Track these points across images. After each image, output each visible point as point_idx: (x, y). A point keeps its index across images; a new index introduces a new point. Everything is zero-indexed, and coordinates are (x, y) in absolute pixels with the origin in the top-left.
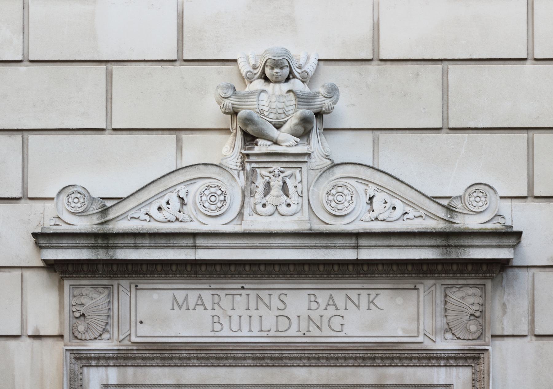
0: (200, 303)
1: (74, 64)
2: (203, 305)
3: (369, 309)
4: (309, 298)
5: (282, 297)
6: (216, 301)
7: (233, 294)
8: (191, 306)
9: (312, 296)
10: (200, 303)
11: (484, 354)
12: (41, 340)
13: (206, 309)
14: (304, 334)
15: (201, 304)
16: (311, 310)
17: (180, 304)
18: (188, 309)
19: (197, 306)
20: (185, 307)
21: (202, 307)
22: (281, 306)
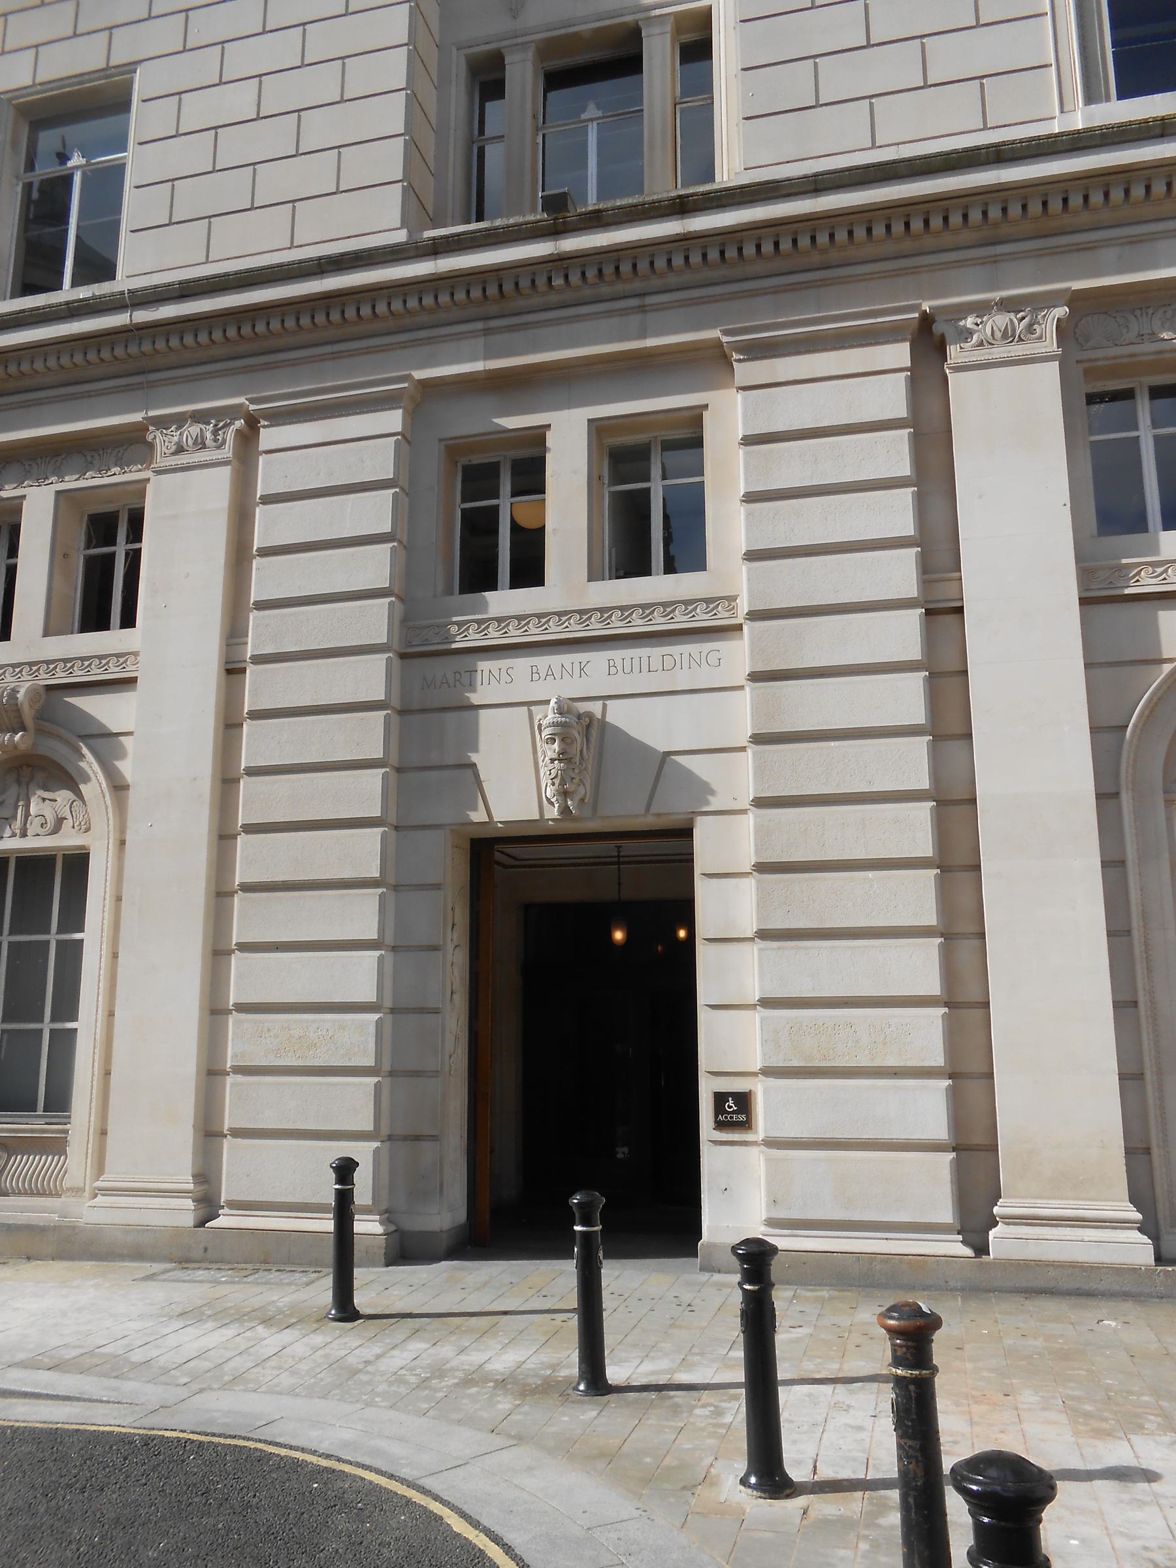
0: (550, 673)
2: (447, 683)
18: (435, 688)
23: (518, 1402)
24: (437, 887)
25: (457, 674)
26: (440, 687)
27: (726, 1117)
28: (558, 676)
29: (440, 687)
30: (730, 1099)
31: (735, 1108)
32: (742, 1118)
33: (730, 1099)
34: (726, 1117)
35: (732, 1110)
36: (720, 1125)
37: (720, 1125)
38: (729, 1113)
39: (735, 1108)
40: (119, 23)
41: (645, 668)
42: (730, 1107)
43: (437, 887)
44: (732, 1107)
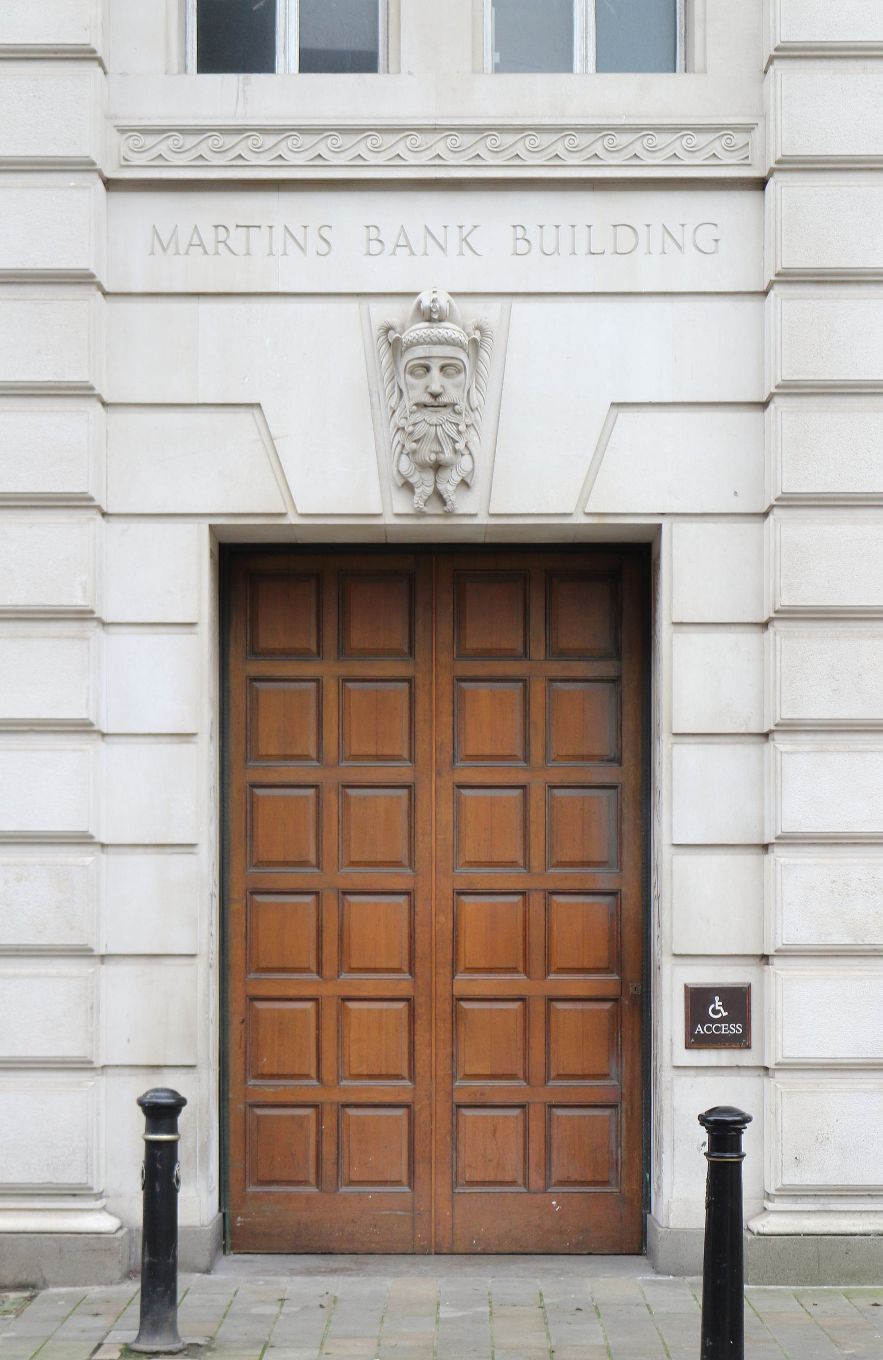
0: (402, 242)
1: (492, 168)
2: (201, 245)
3: (461, 254)
4: (515, 234)
5: (325, 232)
6: (519, 235)
7: (248, 227)
8: (183, 248)
9: (372, 229)
10: (402, 242)
11: (783, 1058)
12: (872, 1198)
13: (412, 253)
14: (435, 396)
15: (199, 243)
16: (517, 254)
17: (165, 244)
18: (177, 253)
19: (398, 249)
20: (171, 249)
21: (406, 249)
22: (324, 248)
23: (91, 970)
24: (186, 737)
25: (372, 229)
26: (187, 253)
27: (709, 1029)
28: (418, 249)
29: (187, 253)
30: (717, 998)
31: (725, 1014)
32: (736, 1029)
33: (717, 998)
34: (709, 1029)
35: (720, 1015)
36: (694, 1041)
37: (694, 1041)
38: (714, 1021)
39: (725, 1014)
40: (169, 1063)
41: (581, 248)
42: (715, 1012)
43: (186, 737)
44: (719, 1011)
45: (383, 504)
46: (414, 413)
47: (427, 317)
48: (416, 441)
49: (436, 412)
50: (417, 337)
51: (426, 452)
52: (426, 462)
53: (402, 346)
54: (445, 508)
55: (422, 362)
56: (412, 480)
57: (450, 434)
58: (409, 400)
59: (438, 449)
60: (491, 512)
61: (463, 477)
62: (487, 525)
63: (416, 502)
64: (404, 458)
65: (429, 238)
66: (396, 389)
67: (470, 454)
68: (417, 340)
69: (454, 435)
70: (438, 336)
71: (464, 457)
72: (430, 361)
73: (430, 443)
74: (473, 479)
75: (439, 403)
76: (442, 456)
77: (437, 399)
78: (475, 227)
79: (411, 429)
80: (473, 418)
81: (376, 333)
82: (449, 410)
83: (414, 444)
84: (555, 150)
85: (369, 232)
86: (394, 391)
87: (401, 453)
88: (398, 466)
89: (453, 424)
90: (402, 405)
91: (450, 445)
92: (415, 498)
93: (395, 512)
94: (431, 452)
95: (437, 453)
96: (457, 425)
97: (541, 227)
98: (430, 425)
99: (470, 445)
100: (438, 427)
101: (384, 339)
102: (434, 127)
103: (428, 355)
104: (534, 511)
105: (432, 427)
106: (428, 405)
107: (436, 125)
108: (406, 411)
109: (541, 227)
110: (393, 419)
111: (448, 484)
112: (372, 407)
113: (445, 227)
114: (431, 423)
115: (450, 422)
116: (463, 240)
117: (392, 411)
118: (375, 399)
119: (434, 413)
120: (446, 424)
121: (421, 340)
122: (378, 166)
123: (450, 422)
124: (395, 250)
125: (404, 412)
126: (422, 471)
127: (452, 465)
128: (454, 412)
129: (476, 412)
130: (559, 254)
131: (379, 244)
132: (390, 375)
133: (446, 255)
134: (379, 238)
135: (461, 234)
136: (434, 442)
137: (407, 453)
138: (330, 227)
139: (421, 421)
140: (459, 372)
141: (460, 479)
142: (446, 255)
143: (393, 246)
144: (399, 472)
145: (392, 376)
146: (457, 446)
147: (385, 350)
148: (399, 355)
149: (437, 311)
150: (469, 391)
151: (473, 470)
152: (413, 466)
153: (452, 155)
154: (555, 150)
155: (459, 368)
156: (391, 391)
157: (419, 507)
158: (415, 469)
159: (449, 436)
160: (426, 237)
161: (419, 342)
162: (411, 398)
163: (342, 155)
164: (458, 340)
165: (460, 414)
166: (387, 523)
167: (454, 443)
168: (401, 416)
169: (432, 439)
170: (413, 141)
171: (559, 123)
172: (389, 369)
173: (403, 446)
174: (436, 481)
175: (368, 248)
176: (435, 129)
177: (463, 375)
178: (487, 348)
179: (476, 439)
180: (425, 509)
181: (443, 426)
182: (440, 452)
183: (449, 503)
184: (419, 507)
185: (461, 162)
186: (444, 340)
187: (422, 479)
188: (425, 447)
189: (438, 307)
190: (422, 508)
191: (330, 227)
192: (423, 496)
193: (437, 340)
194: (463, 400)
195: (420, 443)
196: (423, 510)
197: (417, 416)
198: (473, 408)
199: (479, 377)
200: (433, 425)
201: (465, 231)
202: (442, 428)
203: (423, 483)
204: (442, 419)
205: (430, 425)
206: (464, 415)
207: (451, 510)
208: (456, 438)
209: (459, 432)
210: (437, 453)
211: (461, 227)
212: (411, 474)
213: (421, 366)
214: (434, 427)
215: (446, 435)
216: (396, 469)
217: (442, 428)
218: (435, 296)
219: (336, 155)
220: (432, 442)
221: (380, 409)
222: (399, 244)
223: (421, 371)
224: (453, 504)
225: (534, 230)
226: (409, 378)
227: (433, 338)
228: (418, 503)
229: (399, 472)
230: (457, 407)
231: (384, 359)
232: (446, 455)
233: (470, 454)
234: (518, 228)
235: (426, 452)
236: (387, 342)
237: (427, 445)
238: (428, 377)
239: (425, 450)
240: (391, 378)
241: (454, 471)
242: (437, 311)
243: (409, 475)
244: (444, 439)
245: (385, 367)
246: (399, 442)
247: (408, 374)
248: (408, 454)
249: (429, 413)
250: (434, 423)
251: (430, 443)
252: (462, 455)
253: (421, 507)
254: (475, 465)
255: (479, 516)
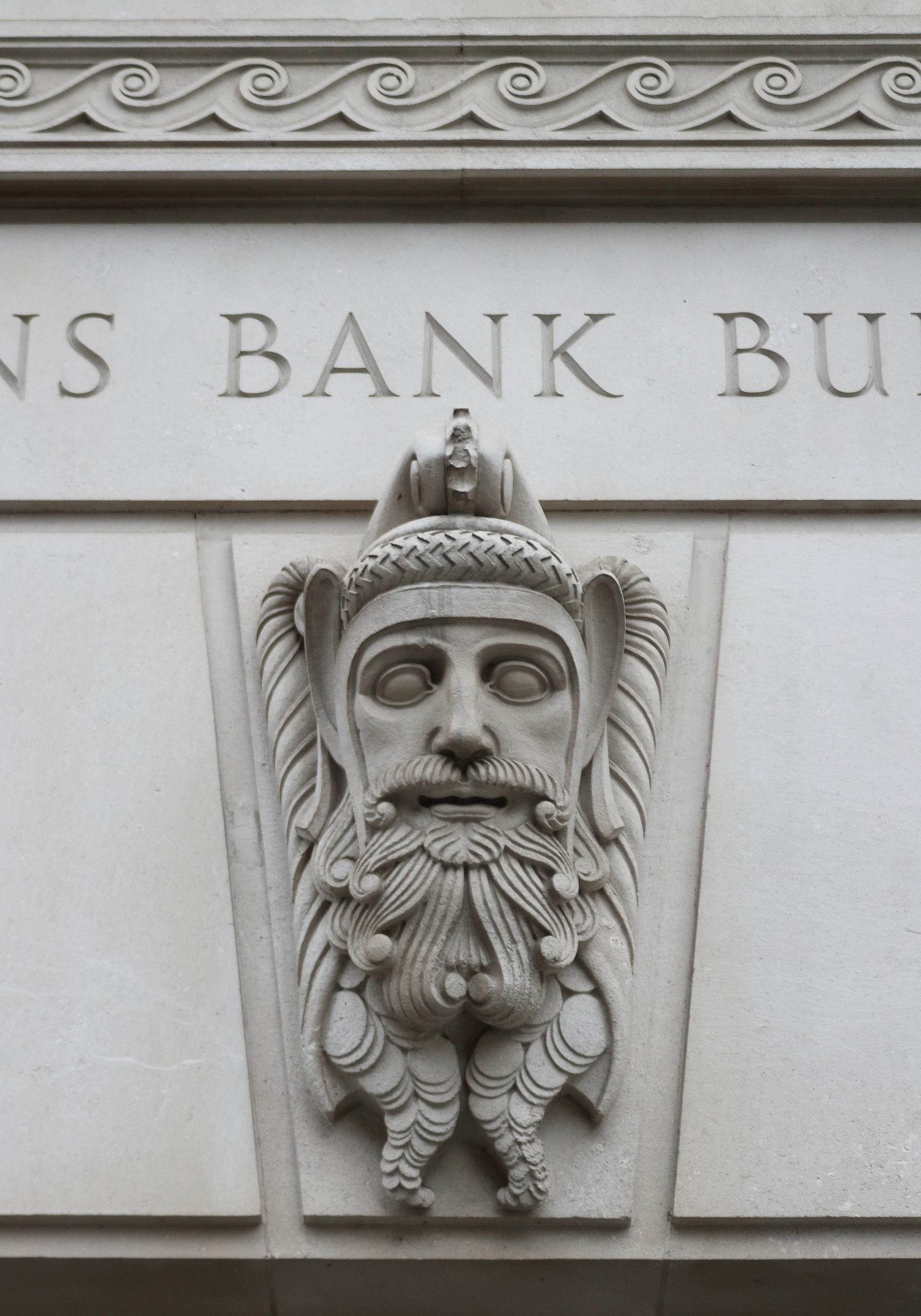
0: (350, 357)
4: (732, 337)
5: (88, 333)
10: (350, 357)
45: (262, 1184)
46: (385, 829)
47: (431, 497)
48: (392, 930)
49: (466, 821)
50: (394, 554)
51: (430, 965)
52: (430, 1004)
53: (342, 599)
54: (503, 1195)
55: (413, 639)
56: (376, 1085)
57: (521, 902)
58: (366, 787)
59: (476, 957)
60: (683, 1210)
61: (572, 1077)
62: (666, 1263)
63: (389, 1168)
64: (346, 1003)
65: (440, 348)
66: (321, 770)
67: (598, 992)
68: (394, 563)
69: (537, 907)
70: (471, 548)
71: (574, 1000)
72: (443, 638)
73: (443, 937)
74: (611, 1088)
75: (478, 784)
76: (491, 982)
77: (472, 772)
78: (596, 318)
79: (372, 883)
80: (605, 866)
81: (251, 611)
82: (517, 819)
83: (384, 939)
84: (855, 103)
85: (239, 335)
86: (312, 789)
87: (336, 987)
88: (321, 1036)
89: (530, 871)
90: (341, 817)
91: (521, 947)
92: (389, 1153)
93: (308, 1212)
94: (450, 969)
95: (470, 973)
96: (547, 872)
97: (818, 318)
98: (447, 867)
99: (596, 958)
100: (473, 876)
101: (282, 626)
102: (457, 43)
103: (435, 613)
104: (847, 1209)
105: (450, 875)
106: (435, 794)
107: (462, 37)
108: (355, 837)
109: (818, 318)
110: (305, 875)
111: (515, 1096)
112: (232, 856)
113: (496, 318)
114: (446, 856)
115: (522, 861)
116: (555, 354)
117: (303, 849)
118: (244, 830)
119: (459, 825)
120: (504, 863)
121: (412, 564)
122: (273, 144)
123: (522, 861)
124: (323, 381)
125: (350, 834)
126: (414, 1050)
127: (529, 1026)
128: (536, 824)
129: (614, 849)
130: (885, 394)
131: (271, 364)
132: (301, 735)
133: (499, 396)
134: (272, 349)
135: (551, 340)
136: (459, 936)
137: (356, 982)
138: (109, 318)
139: (410, 856)
140: (550, 685)
141: (558, 1081)
142: (499, 396)
143: (319, 371)
144: (325, 1058)
145: (307, 739)
146: (548, 946)
147: (282, 659)
148: (332, 632)
149: (470, 467)
150: (586, 773)
151: (608, 1053)
152: (380, 1029)
153: (513, 116)
154: (855, 103)
155: (553, 667)
156: (302, 785)
157: (400, 1186)
158: (387, 1038)
159: (516, 908)
160: (429, 348)
161: (401, 569)
162: (371, 778)
163: (157, 118)
164: (546, 566)
165: (557, 834)
166: (278, 1254)
167: (535, 938)
168: (334, 854)
169: (449, 921)
170: (390, 82)
171: (860, 31)
172: (297, 718)
173: (344, 960)
174: (466, 1091)
175: (235, 376)
176: (461, 50)
177: (563, 700)
178: (649, 653)
179: (615, 940)
180: (426, 1196)
181: (494, 869)
182: (483, 969)
183: (519, 1172)
184: (400, 1186)
185: (547, 134)
186: (495, 562)
187: (415, 1079)
188: (424, 948)
189: (473, 453)
190: (413, 1191)
191: (109, 318)
192: (417, 1143)
193: (470, 561)
194: (566, 786)
195: (405, 937)
196: (417, 1201)
197: (395, 838)
198: (605, 831)
199: (624, 742)
200: (455, 867)
201: (562, 331)
202: (490, 877)
203: (416, 1095)
204: (486, 842)
205: (447, 867)
206: (571, 838)
207: (525, 1200)
208: (545, 917)
209: (555, 900)
210: (470, 973)
211: (547, 319)
212: (371, 1060)
213: (408, 655)
214: (460, 874)
215: (506, 908)
216: (313, 1047)
217: (490, 877)
218: (461, 421)
219: (136, 119)
220: (451, 931)
221: (262, 864)
222: (337, 365)
223: (409, 679)
224: (531, 1174)
225: (794, 326)
226: (365, 706)
227: (453, 556)
228: (397, 1171)
229: (325, 1058)
230: (545, 807)
231: (281, 686)
232: (507, 979)
233: (598, 992)
234: (739, 321)
235: (430, 965)
236: (290, 638)
237: (433, 942)
238: (439, 695)
239: (425, 961)
240: (301, 746)
241: (536, 1049)
242: (470, 467)
243: (364, 1066)
244: (497, 919)
245: (283, 712)
246: (327, 948)
247: (364, 693)
248: (359, 990)
249: (438, 824)
250: (459, 860)
251: (443, 937)
252: (568, 993)
253: (408, 1185)
254: (617, 1036)
255: (636, 1231)
